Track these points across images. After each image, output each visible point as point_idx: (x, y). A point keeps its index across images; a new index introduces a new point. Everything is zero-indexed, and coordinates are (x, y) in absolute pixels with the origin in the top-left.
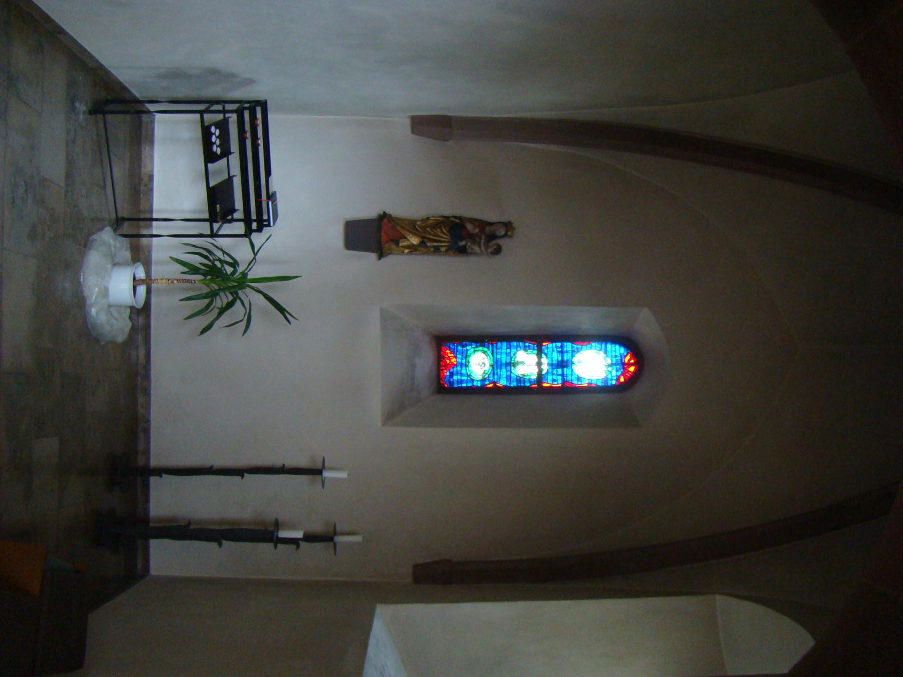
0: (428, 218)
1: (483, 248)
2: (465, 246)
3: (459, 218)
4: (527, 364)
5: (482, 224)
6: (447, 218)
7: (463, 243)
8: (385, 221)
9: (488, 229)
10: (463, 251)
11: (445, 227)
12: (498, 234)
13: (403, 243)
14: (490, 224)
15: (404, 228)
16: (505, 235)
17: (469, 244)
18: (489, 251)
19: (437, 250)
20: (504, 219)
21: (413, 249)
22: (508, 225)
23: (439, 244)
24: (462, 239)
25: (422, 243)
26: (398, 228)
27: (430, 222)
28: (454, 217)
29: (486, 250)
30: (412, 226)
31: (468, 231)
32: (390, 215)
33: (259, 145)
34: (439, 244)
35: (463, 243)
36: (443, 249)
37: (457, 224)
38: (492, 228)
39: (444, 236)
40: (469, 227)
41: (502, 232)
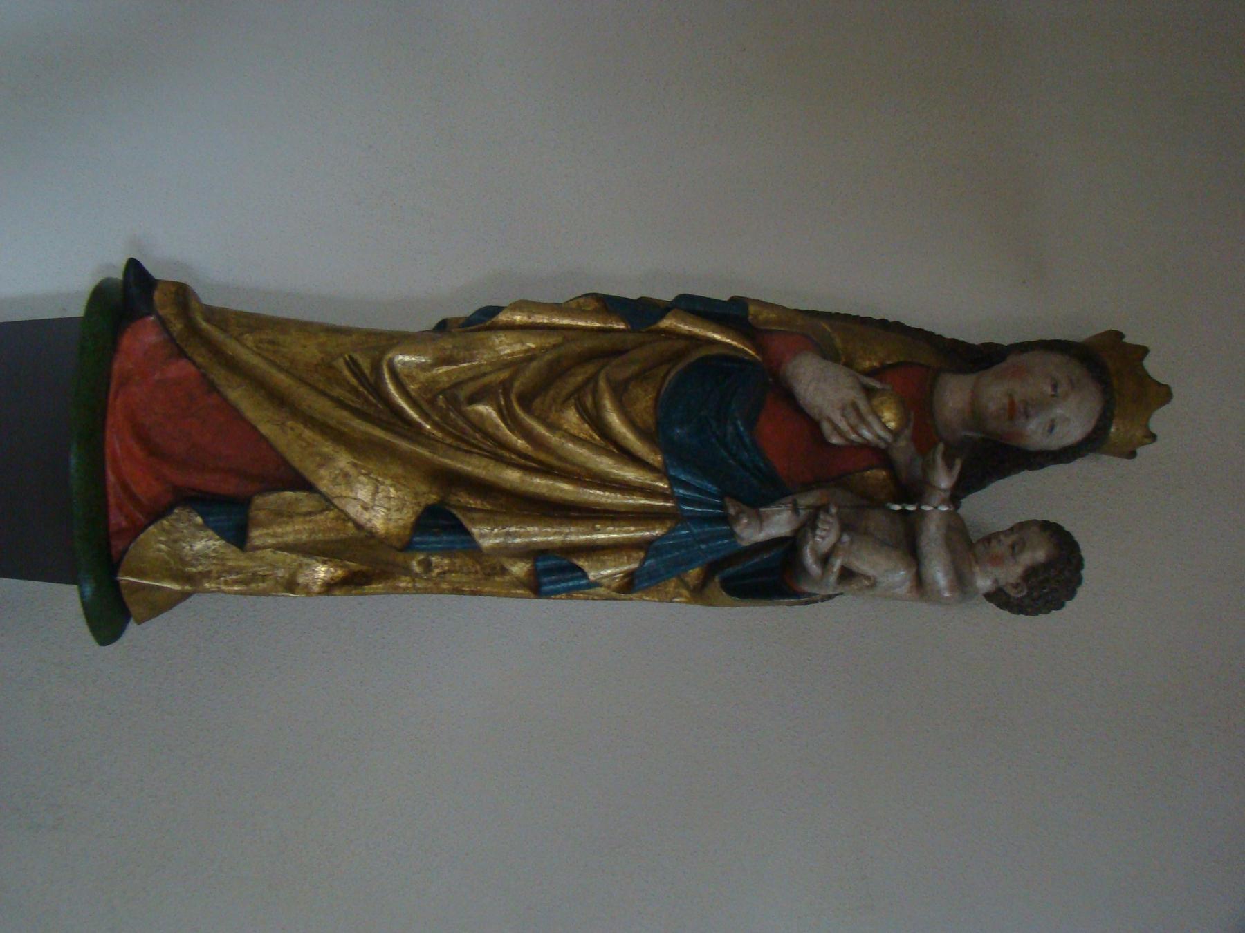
0: (485, 320)
1: (939, 575)
2: (789, 547)
3: (731, 313)
4: (361, 389)
5: (915, 360)
6: (641, 312)
7: (779, 523)
8: (143, 337)
9: (954, 396)
10: (770, 577)
11: (620, 393)
12: (1035, 433)
13: (279, 526)
14: (979, 358)
15: (279, 400)
16: (1094, 442)
17: (825, 537)
18: (984, 583)
19: (554, 573)
20: (1078, 317)
21: (366, 564)
22: (1114, 374)
23: (577, 535)
24: (760, 496)
25: (438, 524)
26: (238, 395)
27: (507, 347)
28: (691, 305)
29: (961, 582)
30: (350, 380)
31: (812, 425)
32: (182, 294)
33: (426, 421)
34: (577, 535)
35: (779, 523)
36: (608, 571)
37: (721, 366)
38: (995, 392)
39: (616, 464)
40: (822, 388)
41: (1072, 419)
